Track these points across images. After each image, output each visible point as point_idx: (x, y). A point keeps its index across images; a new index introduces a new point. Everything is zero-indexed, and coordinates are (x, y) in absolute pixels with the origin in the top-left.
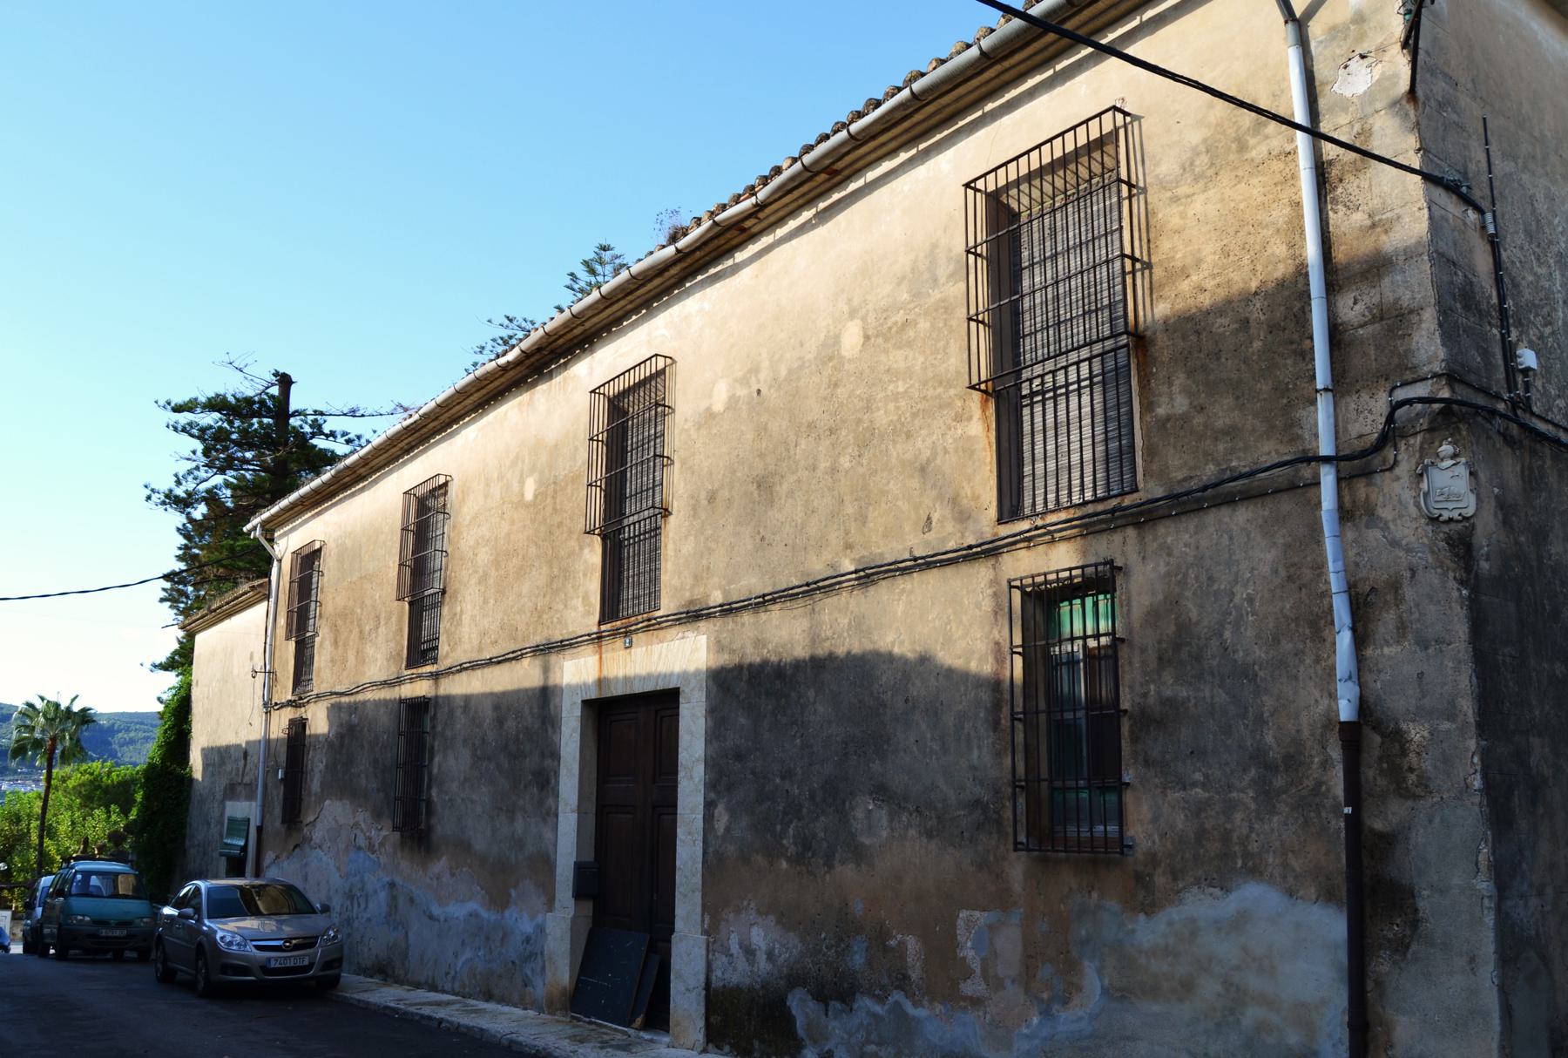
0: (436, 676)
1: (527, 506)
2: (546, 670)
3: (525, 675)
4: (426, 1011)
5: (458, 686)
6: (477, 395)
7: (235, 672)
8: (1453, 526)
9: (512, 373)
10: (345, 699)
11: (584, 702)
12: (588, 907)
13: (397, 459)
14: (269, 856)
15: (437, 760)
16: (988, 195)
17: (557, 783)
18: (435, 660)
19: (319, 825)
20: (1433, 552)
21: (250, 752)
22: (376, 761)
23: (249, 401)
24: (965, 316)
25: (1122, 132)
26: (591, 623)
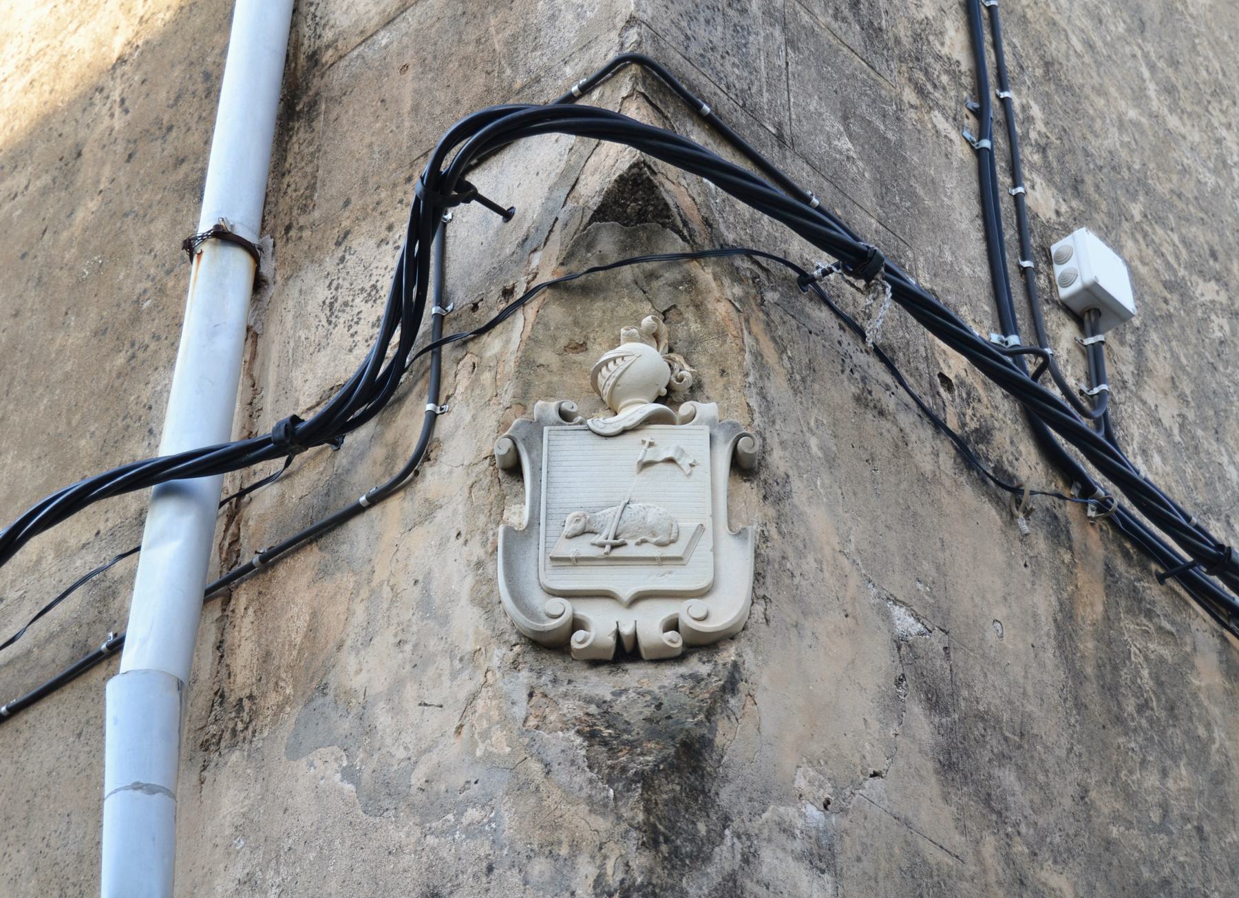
8: (634, 676)
20: (522, 787)
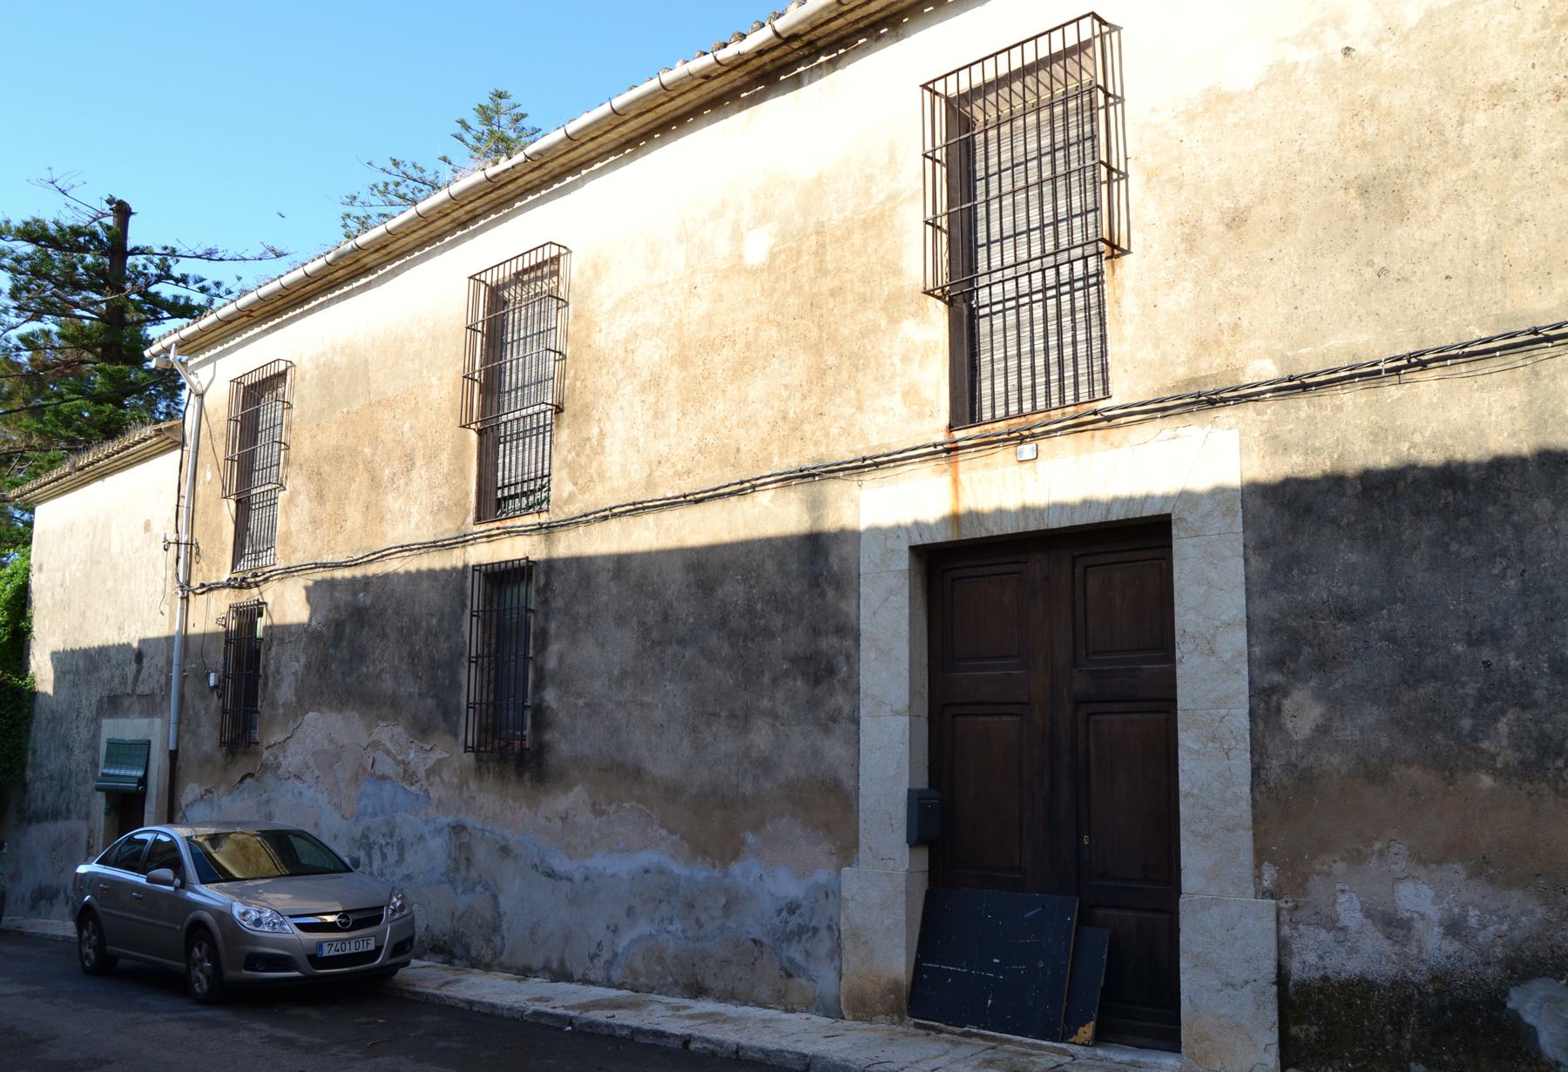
0: (547, 529)
1: (753, 272)
2: (815, 506)
3: (776, 516)
4: (599, 1016)
5: (569, 545)
6: (634, 124)
7: (115, 549)
9: (715, 84)
10: (339, 574)
11: (914, 550)
12: (923, 854)
13: (440, 237)
14: (190, 792)
15: (554, 648)
16: (948, 100)
17: (854, 672)
18: (538, 506)
19: (293, 746)
21: (144, 649)
22: (414, 656)
23: (76, 231)
24: (921, 219)
25: (1098, 41)
26: (935, 425)
